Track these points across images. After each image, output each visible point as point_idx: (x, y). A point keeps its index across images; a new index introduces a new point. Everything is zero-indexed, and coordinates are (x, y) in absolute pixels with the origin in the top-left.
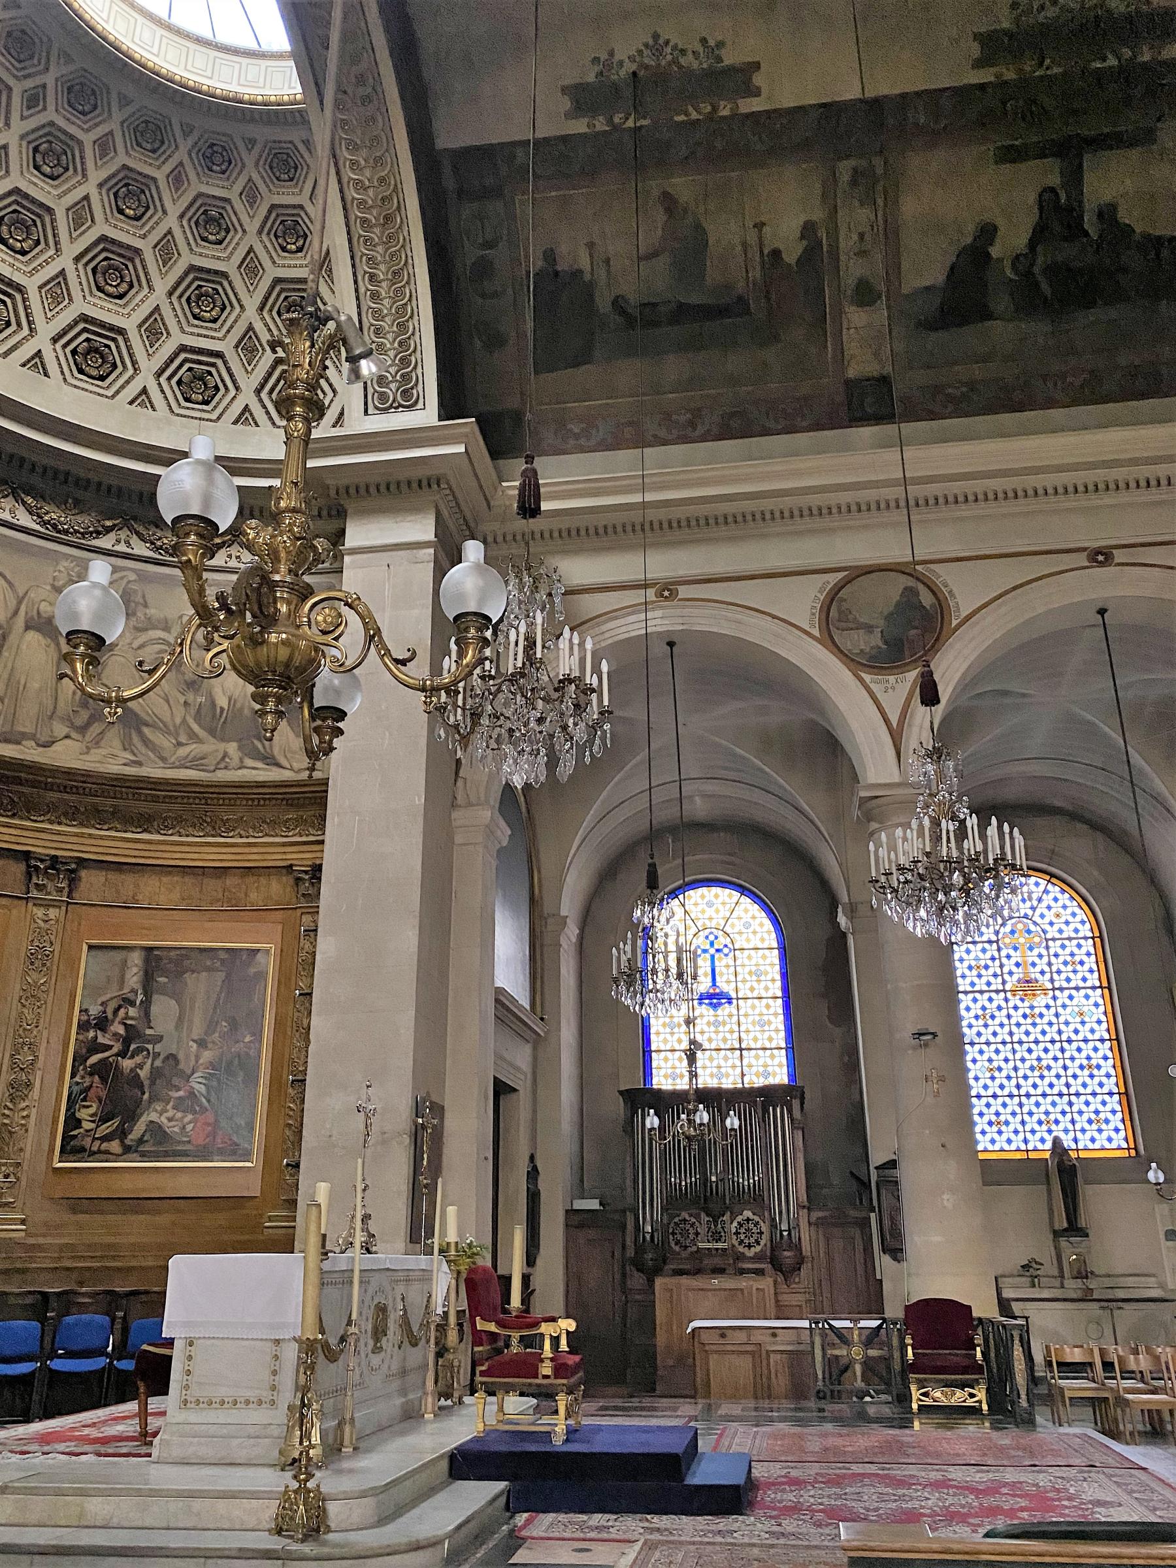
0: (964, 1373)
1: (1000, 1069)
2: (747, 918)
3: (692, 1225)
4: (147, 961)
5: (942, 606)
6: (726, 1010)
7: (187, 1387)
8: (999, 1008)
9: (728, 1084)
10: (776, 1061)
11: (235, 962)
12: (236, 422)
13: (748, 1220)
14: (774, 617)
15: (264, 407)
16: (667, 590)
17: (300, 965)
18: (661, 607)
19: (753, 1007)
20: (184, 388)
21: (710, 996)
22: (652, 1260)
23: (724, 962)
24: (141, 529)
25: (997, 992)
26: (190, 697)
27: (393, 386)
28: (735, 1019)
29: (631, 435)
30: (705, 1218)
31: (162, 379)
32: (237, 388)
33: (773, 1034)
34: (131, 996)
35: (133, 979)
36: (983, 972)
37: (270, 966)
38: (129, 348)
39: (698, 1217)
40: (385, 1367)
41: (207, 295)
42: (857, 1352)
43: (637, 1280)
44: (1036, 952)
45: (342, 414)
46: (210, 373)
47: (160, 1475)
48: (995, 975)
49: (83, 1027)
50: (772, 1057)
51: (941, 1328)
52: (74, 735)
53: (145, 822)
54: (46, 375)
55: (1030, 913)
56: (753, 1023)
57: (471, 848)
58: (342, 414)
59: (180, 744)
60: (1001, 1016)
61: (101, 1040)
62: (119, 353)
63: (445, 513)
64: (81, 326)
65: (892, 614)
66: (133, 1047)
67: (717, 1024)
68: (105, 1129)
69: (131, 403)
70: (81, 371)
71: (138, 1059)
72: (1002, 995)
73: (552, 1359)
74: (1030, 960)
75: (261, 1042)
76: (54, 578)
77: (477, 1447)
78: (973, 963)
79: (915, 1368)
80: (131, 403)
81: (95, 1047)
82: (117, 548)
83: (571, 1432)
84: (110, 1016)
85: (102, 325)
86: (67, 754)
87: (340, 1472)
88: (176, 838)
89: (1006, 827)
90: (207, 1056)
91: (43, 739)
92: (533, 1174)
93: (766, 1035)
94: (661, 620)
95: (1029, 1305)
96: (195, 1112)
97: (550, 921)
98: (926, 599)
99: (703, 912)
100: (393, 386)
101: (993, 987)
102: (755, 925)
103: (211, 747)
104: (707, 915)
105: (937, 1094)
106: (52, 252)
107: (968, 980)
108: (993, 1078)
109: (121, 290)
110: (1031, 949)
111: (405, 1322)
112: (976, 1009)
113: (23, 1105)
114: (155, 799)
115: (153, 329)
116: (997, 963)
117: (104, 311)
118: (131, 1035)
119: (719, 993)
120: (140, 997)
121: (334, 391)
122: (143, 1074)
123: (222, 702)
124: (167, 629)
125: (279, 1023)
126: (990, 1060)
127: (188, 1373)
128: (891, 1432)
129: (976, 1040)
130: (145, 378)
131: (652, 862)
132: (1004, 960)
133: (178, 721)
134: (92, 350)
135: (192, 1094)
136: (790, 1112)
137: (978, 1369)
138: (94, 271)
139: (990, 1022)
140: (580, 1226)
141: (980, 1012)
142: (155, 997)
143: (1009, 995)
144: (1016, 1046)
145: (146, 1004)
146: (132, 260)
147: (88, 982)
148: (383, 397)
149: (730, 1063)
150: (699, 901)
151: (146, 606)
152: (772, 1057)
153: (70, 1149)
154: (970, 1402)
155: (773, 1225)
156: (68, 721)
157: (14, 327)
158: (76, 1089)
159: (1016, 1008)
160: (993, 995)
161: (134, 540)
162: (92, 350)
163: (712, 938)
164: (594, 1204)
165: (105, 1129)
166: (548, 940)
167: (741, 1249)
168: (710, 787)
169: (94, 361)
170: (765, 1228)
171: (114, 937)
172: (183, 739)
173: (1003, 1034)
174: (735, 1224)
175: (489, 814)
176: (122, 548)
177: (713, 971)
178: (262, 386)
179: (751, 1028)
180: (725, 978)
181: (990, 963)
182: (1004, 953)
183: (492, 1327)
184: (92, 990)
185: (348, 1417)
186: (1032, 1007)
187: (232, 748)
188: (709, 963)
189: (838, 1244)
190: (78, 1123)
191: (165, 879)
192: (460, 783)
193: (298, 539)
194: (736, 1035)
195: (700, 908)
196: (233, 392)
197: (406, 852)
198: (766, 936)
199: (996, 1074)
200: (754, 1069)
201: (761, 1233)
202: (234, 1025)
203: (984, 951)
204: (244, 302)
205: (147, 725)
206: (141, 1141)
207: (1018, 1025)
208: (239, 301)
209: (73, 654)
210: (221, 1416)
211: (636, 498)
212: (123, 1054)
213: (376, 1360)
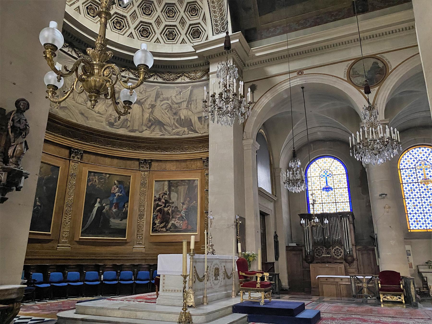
0: (397, 291)
1: (417, 205)
2: (336, 166)
3: (321, 250)
4: (169, 184)
5: (385, 65)
6: (331, 192)
7: (164, 287)
8: (416, 188)
9: (332, 212)
10: (347, 205)
11: (190, 183)
12: (181, 43)
13: (337, 249)
14: (333, 76)
15: (188, 38)
16: (300, 72)
17: (205, 183)
18: (299, 77)
19: (339, 191)
21: (326, 188)
22: (310, 259)
23: (330, 179)
24: (159, 75)
25: (416, 183)
26: (175, 117)
27: (220, 26)
28: (334, 194)
29: (288, 29)
30: (325, 248)
31: (162, 35)
32: (181, 34)
33: (345, 198)
34: (166, 193)
35: (166, 188)
36: (411, 177)
37: (199, 183)
38: (153, 28)
39: (323, 248)
40: (219, 283)
41: (171, 10)
42: (365, 285)
43: (306, 264)
44: (428, 170)
45: (207, 36)
46: (173, 31)
47: (159, 308)
48: (415, 178)
49: (155, 200)
50: (345, 204)
51: (391, 280)
52: (148, 129)
53: (166, 149)
54: (134, 38)
55: (426, 159)
56: (339, 195)
57: (248, 151)
58: (207, 36)
59: (173, 129)
61: (159, 204)
63: (236, 59)
64: (115, 15)
65: (370, 71)
66: (167, 205)
67: (328, 196)
68: (162, 225)
69: (155, 42)
70: (142, 36)
71: (169, 208)
72: (417, 184)
73: (260, 283)
74: (426, 173)
75: (197, 203)
76: (140, 90)
77: (240, 305)
78: (407, 175)
79: (381, 290)
80: (155, 42)
81: (158, 205)
82: (154, 80)
83: (266, 303)
84: (161, 197)
85: (146, 23)
86: (147, 134)
87: (200, 309)
88: (174, 153)
90: (185, 206)
91: (141, 130)
92: (276, 237)
93: (343, 198)
94: (297, 82)
95: (428, 274)
96: (182, 221)
97: (277, 170)
98: (381, 65)
99: (323, 165)
100: (220, 26)
101: (414, 182)
102: (339, 168)
103: (181, 129)
104: (324, 166)
105: (388, 212)
106: (132, 6)
107: (406, 180)
108: (415, 208)
109: (150, 13)
110: (426, 169)
112: (409, 188)
113: (143, 220)
114: (169, 144)
115: (158, 21)
116: (415, 174)
117: (146, 19)
118: (167, 202)
119: (327, 186)
120: (168, 193)
121: (205, 31)
122: (170, 211)
123: (183, 117)
124: (168, 100)
125: (202, 198)
126: (414, 203)
127: (164, 283)
128: (371, 307)
129: (409, 197)
130: (158, 35)
131: (307, 151)
132: (418, 173)
133: (172, 123)
134: (144, 30)
135: (182, 216)
136: (349, 219)
137: (402, 291)
138: (142, 9)
139: (413, 192)
141: (410, 189)
142: (171, 193)
143: (419, 183)
144: (422, 199)
145: (170, 195)
146: (151, 4)
147: (156, 190)
148: (217, 30)
149: (333, 206)
150: (322, 162)
151: (162, 95)
152: (345, 204)
153: (154, 230)
154: (399, 300)
155: (345, 250)
156: (146, 125)
157: (125, 27)
158: (154, 216)
159: (422, 187)
160: (414, 184)
161: (158, 78)
162: (118, 22)
163: (326, 172)
164: (294, 245)
165: (162, 225)
166: (276, 175)
167: (336, 256)
168: (323, 129)
169: (145, 33)
170: (342, 251)
171: (162, 178)
172: (174, 128)
173: (418, 195)
174: (334, 250)
175: (252, 141)
176: (155, 80)
177: (327, 181)
178: (187, 32)
179: (338, 197)
180: (330, 183)
181: (413, 174)
182: (417, 171)
183: (244, 274)
184: (157, 191)
185: (205, 296)
186: (427, 187)
187: (186, 129)
188: (325, 179)
189: (365, 256)
190: (155, 224)
191: (172, 163)
192: (244, 133)
194: (334, 199)
195: (322, 164)
196: (180, 35)
197: (229, 152)
198: (342, 171)
199: (416, 207)
200: (340, 208)
201: (341, 252)
202: (191, 198)
203: (411, 171)
204: (180, 10)
205: (165, 125)
206: (170, 228)
207: (423, 192)
208: (179, 10)
210: (173, 294)
212: (165, 207)
213: (216, 282)
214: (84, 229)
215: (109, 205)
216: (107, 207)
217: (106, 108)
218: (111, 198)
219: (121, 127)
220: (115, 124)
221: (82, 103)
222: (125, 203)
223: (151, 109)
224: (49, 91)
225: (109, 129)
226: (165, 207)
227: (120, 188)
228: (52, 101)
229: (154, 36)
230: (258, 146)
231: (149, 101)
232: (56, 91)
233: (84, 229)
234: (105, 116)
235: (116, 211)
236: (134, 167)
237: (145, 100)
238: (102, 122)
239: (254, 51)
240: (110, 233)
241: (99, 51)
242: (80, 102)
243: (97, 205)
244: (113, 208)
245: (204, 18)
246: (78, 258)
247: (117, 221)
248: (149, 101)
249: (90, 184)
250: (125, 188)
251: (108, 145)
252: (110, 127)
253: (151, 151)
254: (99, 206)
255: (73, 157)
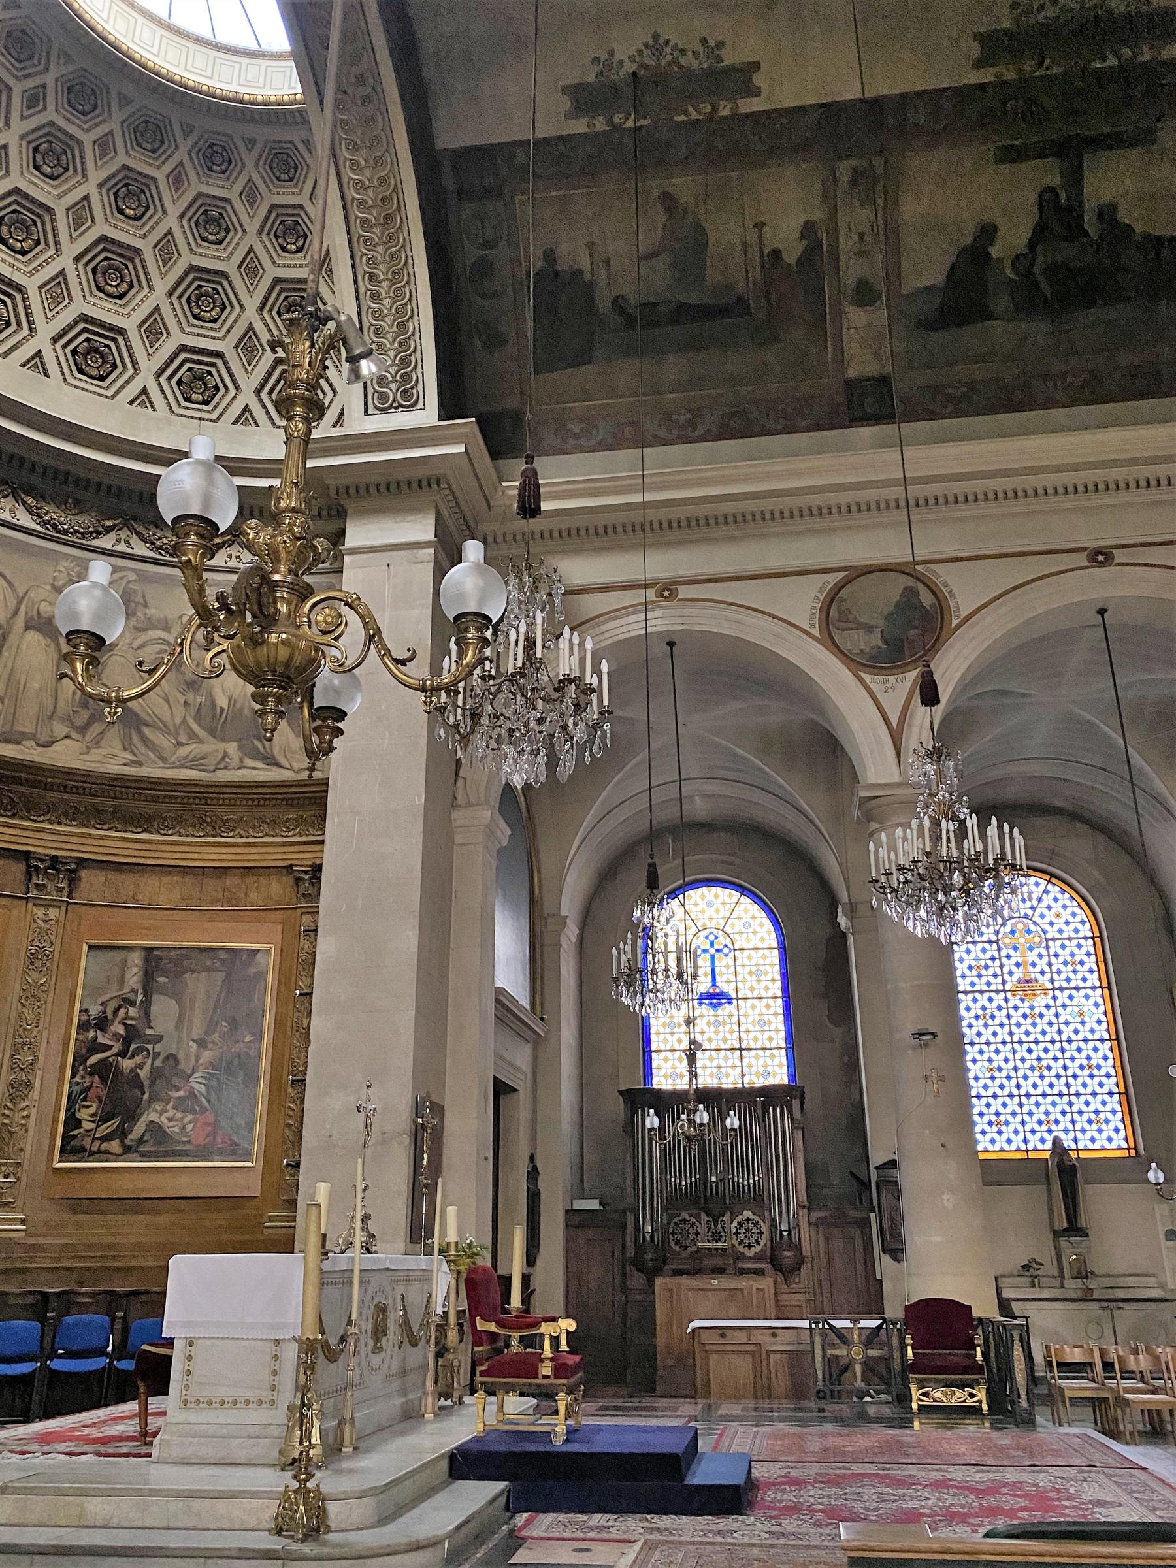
0: (964, 1373)
1: (1000, 1069)
2: (747, 918)
3: (692, 1225)
4: (147, 961)
5: (942, 606)
6: (726, 1010)
7: (187, 1387)
8: (999, 1008)
9: (728, 1084)
10: (776, 1061)
11: (235, 962)
12: (236, 422)
13: (748, 1220)
14: (774, 617)
15: (264, 407)
16: (667, 590)
17: (300, 965)
18: (661, 607)
19: (753, 1007)
20: (184, 388)
21: (710, 996)
22: (652, 1260)
23: (724, 962)
24: (141, 529)
25: (997, 992)
26: (190, 697)
27: (393, 386)
28: (735, 1019)
29: (631, 435)
30: (705, 1218)
31: (162, 379)
32: (237, 388)
33: (773, 1034)
34: (131, 996)
35: (133, 979)
36: (983, 972)
37: (270, 966)
38: (129, 348)
39: (698, 1217)
40: (385, 1367)
41: (207, 295)
42: (857, 1352)
43: (637, 1280)
44: (1036, 952)
45: (342, 414)
46: (210, 373)
47: (160, 1475)
48: (995, 975)
49: (83, 1027)
50: (772, 1057)
51: (941, 1328)
52: (74, 735)
53: (145, 822)
54: (46, 375)
55: (1030, 913)
56: (753, 1023)
57: (471, 848)
58: (342, 414)
59: (180, 744)
61: (101, 1040)
62: (119, 353)
63: (445, 513)
64: (81, 326)
65: (892, 614)
66: (133, 1047)
67: (717, 1024)
68: (105, 1129)
69: (131, 403)
70: (81, 371)
71: (138, 1059)
72: (1002, 995)
73: (552, 1359)
74: (1030, 960)
75: (261, 1042)
76: (54, 578)
77: (477, 1447)
78: (973, 963)
79: (915, 1368)
80: (131, 403)
81: (95, 1047)
82: (117, 548)
83: (571, 1432)
84: (110, 1016)
85: (102, 325)
86: (67, 754)
87: (340, 1472)
88: (176, 838)
90: (207, 1056)
91: (43, 739)
92: (533, 1174)
93: (766, 1035)
94: (661, 620)
95: (1029, 1305)
96: (195, 1112)
97: (550, 921)
98: (926, 599)
99: (703, 912)
100: (393, 386)
101: (993, 987)
102: (755, 925)
103: (211, 747)
104: (707, 915)
105: (937, 1094)
106: (52, 252)
107: (968, 980)
108: (993, 1078)
109: (121, 290)
110: (1031, 949)
112: (976, 1009)
113: (23, 1105)
114: (155, 799)
115: (153, 329)
116: (997, 963)
117: (104, 311)
118: (131, 1035)
119: (719, 993)
120: (140, 997)
121: (334, 391)
122: (143, 1074)
123: (222, 702)
124: (167, 629)
125: (279, 1023)
126: (990, 1060)
127: (188, 1373)
128: (891, 1432)
129: (976, 1040)
130: (145, 378)
131: (652, 862)
132: (1004, 960)
133: (178, 721)
134: (92, 350)
135: (192, 1094)
136: (790, 1112)
137: (978, 1369)
138: (94, 271)
139: (990, 1022)
140: (580, 1226)
141: (980, 1012)
142: (155, 997)
143: (1009, 995)
144: (1016, 1046)
145: (146, 1004)
146: (132, 260)
147: (88, 982)
148: (383, 397)
149: (730, 1063)
150: (699, 901)
151: (146, 606)
152: (772, 1057)
153: (70, 1149)
154: (970, 1402)
155: (773, 1225)
156: (68, 721)
157: (14, 327)
158: (76, 1089)
159: (1016, 1008)
160: (993, 995)
161: (134, 540)
163: (712, 938)
164: (594, 1204)
165: (105, 1129)
166: (548, 940)
167: (741, 1249)
168: (710, 787)
169: (94, 361)
170: (765, 1228)
171: (114, 937)
172: (183, 739)
173: (1003, 1034)
174: (735, 1224)
175: (489, 814)
176: (122, 548)
177: (713, 971)
178: (262, 386)
179: (751, 1028)
180: (725, 978)
181: (990, 963)
182: (1004, 953)
183: (492, 1327)
185: (348, 1417)
186: (1032, 1007)
187: (232, 748)
188: (709, 963)
189: (838, 1244)
190: (78, 1123)
191: (165, 879)
192: (460, 783)
194: (736, 1035)
195: (700, 908)
196: (233, 392)
197: (406, 852)
198: (766, 936)
199: (996, 1074)
200: (754, 1069)
201: (761, 1233)
202: (234, 1025)
203: (984, 951)
204: (244, 302)
205: (147, 725)
206: (141, 1141)
207: (1018, 1025)
208: (239, 301)
210: (221, 1416)
212: (123, 1054)
213: (376, 1360)
224: (73, 654)
228: (91, 696)
230: (504, 832)
232: (340, 725)
241: (298, 539)
253: (81, 825)
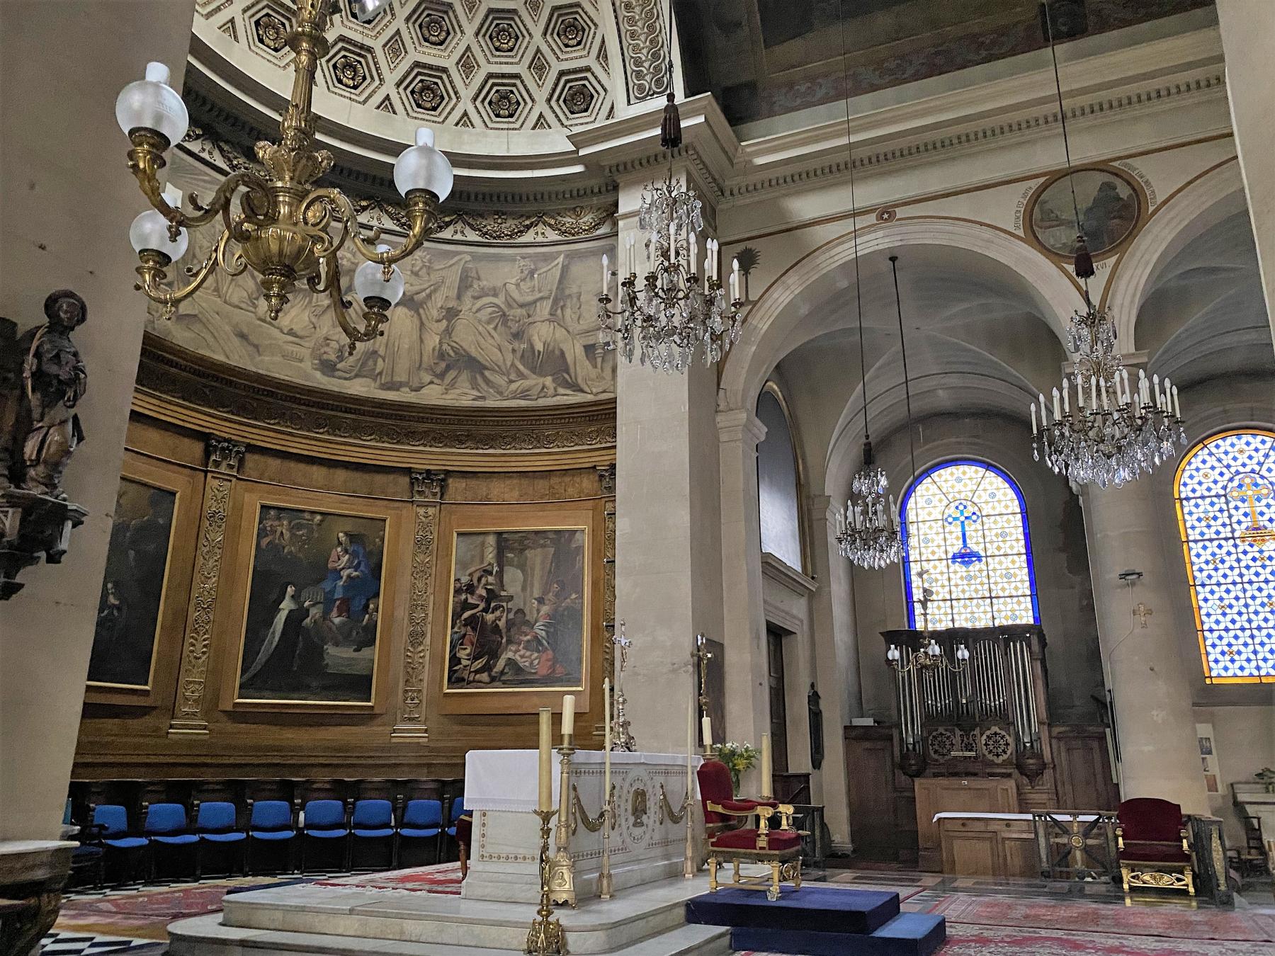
0: (1173, 860)
1: (1231, 606)
2: (991, 489)
3: (948, 738)
4: (499, 543)
5: (1137, 192)
6: (976, 566)
7: (483, 846)
8: (1229, 553)
9: (980, 625)
10: (1023, 606)
11: (562, 539)
12: (534, 128)
13: (996, 734)
14: (982, 224)
15: (554, 112)
16: (886, 213)
17: (605, 540)
18: (882, 228)
19: (1000, 563)
21: (962, 556)
22: (916, 764)
23: (973, 527)
24: (471, 221)
25: (1226, 539)
26: (516, 345)
27: (648, 78)
28: (985, 573)
29: (850, 86)
30: (958, 733)
31: (478, 103)
32: (533, 100)
33: (1019, 585)
34: (489, 568)
35: (490, 556)
36: (1212, 523)
37: (586, 541)
38: (451, 82)
39: (953, 731)
40: (648, 836)
41: (504, 30)
42: (1077, 841)
43: (903, 779)
44: (1264, 502)
45: (612, 108)
46: (512, 92)
47: (468, 909)
48: (1224, 525)
49: (458, 592)
50: (1019, 603)
51: (1154, 826)
52: (436, 381)
53: (489, 441)
54: (394, 112)
55: (1257, 468)
56: (1001, 576)
57: (732, 444)
58: (612, 108)
59: (511, 381)
60: (1231, 561)
61: (470, 601)
63: (695, 174)
64: (340, 45)
65: (1091, 209)
66: (493, 605)
67: (969, 578)
68: (478, 664)
69: (457, 124)
70: (419, 106)
71: (498, 613)
72: (1231, 542)
73: (767, 835)
74: (1258, 510)
75: (582, 598)
77: (708, 900)
78: (1202, 516)
79: (1124, 855)
80: (457, 124)
81: (466, 606)
82: (456, 237)
83: (785, 893)
84: (475, 582)
85: (431, 67)
86: (433, 395)
87: (590, 912)
88: (513, 451)
89: (1156, 379)
90: (545, 609)
91: (416, 385)
92: (814, 698)
93: (1013, 585)
94: (878, 241)
95: (1262, 808)
96: (538, 651)
97: (816, 500)
98: (1124, 192)
99: (953, 487)
100: (648, 78)
101: (1222, 536)
102: (999, 495)
103: (533, 381)
104: (956, 490)
105: (1144, 626)
106: (389, 17)
107: (1198, 531)
108: (1224, 614)
109: (442, 38)
110: (1259, 500)
111: (665, 804)
112: (1206, 555)
113: (421, 648)
114: (498, 424)
115: (467, 63)
116: (1226, 514)
117: (431, 56)
118: (492, 595)
119: (965, 549)
120: (496, 569)
121: (605, 90)
122: (502, 624)
123: (539, 346)
124: (495, 295)
125: (595, 584)
126: (1221, 599)
127: (483, 836)
128: (1094, 906)
129: (1207, 582)
130: (466, 104)
131: (905, 446)
132: (1233, 512)
133: (509, 364)
134: (426, 88)
135: (536, 637)
136: (1029, 646)
137: (1187, 858)
138: (420, 26)
139: (1220, 566)
141: (1210, 558)
142: (506, 568)
143: (1238, 541)
144: (1247, 586)
145: (500, 574)
146: (446, 13)
147: (459, 561)
148: (641, 88)
149: (982, 609)
150: (949, 478)
151: (479, 279)
152: (1019, 603)
153: (455, 680)
154: (1177, 885)
155: (1017, 739)
156: (431, 370)
157: (369, 80)
158: (456, 636)
159: (1245, 553)
160: (1223, 542)
161: (467, 230)
163: (961, 507)
164: (869, 722)
165: (478, 664)
166: (816, 515)
167: (990, 757)
168: (953, 380)
169: (428, 96)
170: (1010, 740)
171: (477, 525)
172: (513, 377)
173: (1233, 576)
174: (984, 737)
175: (745, 415)
176: (458, 237)
177: (964, 535)
178: (552, 95)
179: (999, 580)
180: (974, 540)
181: (1218, 514)
182: (1232, 505)
183: (719, 809)
185: (606, 872)
186: (1261, 552)
187: (548, 381)
188: (960, 529)
189: (1078, 755)
190: (459, 661)
191: (508, 482)
192: (721, 392)
193: (293, 150)
194: (986, 587)
195: (950, 484)
196: (530, 104)
197: (675, 449)
198: (1009, 503)
199: (1228, 611)
200: (1003, 614)
201: (1007, 744)
202: (562, 586)
203: (1212, 504)
204: (531, 31)
205: (487, 369)
206: (502, 673)
207: (1248, 567)
208: (527, 30)
209: (143, 268)
210: (510, 868)
211: (843, 141)
212: (486, 610)
213: (638, 831)
214: (247, 676)
215: (321, 606)
216: (315, 612)
217: (314, 320)
218: (327, 585)
219: (356, 376)
220: (339, 366)
221: (243, 305)
222: (368, 600)
223: (445, 323)
225: (321, 381)
226: (486, 610)
227: (354, 555)
229: (455, 105)
231: (439, 299)
233: (247, 676)
234: (309, 344)
235: (343, 624)
236: (394, 494)
237: (429, 296)
238: (301, 361)
239: (748, 150)
240: (325, 688)
242: (235, 300)
243: (287, 605)
244: (335, 613)
245: (603, 54)
246: (232, 761)
247: (346, 653)
248: (439, 299)
249: (265, 542)
250: (369, 554)
251: (319, 426)
252: (324, 373)
254: (293, 606)
255: (217, 464)
